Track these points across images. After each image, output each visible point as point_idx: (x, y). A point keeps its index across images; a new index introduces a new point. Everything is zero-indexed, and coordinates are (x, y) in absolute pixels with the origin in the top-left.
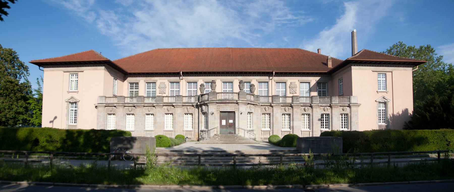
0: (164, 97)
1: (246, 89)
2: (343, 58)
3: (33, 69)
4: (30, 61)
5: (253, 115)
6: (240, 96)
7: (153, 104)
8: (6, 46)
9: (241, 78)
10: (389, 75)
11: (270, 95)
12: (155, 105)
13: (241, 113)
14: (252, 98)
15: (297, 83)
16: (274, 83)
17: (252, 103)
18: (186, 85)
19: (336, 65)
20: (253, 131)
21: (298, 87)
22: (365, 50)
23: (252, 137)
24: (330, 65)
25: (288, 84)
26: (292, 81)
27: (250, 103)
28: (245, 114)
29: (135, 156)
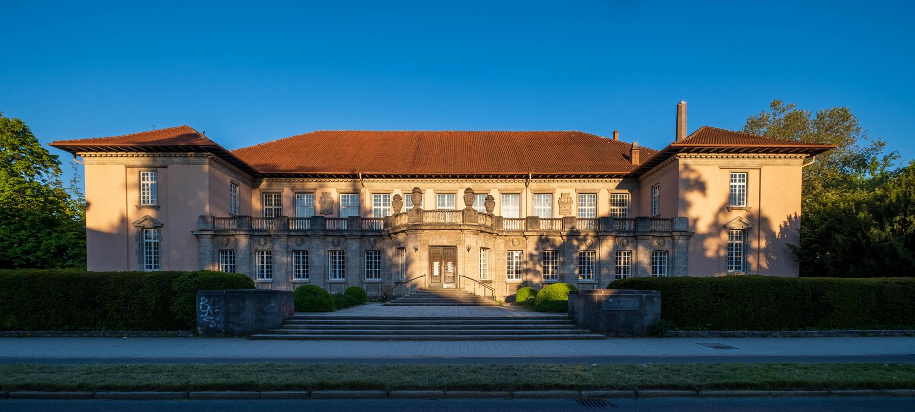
0: (326, 219)
1: (479, 205)
2: (658, 147)
4: (51, 143)
5: (490, 254)
6: (467, 218)
8: (11, 116)
9: (468, 184)
10: (753, 175)
11: (524, 216)
12: (309, 233)
13: (468, 250)
14: (489, 222)
15: (574, 196)
16: (530, 194)
17: (488, 230)
18: (371, 199)
20: (490, 282)
21: (575, 202)
22: (707, 128)
23: (489, 293)
24: (636, 161)
25: (557, 196)
26: (564, 191)
28: (475, 253)
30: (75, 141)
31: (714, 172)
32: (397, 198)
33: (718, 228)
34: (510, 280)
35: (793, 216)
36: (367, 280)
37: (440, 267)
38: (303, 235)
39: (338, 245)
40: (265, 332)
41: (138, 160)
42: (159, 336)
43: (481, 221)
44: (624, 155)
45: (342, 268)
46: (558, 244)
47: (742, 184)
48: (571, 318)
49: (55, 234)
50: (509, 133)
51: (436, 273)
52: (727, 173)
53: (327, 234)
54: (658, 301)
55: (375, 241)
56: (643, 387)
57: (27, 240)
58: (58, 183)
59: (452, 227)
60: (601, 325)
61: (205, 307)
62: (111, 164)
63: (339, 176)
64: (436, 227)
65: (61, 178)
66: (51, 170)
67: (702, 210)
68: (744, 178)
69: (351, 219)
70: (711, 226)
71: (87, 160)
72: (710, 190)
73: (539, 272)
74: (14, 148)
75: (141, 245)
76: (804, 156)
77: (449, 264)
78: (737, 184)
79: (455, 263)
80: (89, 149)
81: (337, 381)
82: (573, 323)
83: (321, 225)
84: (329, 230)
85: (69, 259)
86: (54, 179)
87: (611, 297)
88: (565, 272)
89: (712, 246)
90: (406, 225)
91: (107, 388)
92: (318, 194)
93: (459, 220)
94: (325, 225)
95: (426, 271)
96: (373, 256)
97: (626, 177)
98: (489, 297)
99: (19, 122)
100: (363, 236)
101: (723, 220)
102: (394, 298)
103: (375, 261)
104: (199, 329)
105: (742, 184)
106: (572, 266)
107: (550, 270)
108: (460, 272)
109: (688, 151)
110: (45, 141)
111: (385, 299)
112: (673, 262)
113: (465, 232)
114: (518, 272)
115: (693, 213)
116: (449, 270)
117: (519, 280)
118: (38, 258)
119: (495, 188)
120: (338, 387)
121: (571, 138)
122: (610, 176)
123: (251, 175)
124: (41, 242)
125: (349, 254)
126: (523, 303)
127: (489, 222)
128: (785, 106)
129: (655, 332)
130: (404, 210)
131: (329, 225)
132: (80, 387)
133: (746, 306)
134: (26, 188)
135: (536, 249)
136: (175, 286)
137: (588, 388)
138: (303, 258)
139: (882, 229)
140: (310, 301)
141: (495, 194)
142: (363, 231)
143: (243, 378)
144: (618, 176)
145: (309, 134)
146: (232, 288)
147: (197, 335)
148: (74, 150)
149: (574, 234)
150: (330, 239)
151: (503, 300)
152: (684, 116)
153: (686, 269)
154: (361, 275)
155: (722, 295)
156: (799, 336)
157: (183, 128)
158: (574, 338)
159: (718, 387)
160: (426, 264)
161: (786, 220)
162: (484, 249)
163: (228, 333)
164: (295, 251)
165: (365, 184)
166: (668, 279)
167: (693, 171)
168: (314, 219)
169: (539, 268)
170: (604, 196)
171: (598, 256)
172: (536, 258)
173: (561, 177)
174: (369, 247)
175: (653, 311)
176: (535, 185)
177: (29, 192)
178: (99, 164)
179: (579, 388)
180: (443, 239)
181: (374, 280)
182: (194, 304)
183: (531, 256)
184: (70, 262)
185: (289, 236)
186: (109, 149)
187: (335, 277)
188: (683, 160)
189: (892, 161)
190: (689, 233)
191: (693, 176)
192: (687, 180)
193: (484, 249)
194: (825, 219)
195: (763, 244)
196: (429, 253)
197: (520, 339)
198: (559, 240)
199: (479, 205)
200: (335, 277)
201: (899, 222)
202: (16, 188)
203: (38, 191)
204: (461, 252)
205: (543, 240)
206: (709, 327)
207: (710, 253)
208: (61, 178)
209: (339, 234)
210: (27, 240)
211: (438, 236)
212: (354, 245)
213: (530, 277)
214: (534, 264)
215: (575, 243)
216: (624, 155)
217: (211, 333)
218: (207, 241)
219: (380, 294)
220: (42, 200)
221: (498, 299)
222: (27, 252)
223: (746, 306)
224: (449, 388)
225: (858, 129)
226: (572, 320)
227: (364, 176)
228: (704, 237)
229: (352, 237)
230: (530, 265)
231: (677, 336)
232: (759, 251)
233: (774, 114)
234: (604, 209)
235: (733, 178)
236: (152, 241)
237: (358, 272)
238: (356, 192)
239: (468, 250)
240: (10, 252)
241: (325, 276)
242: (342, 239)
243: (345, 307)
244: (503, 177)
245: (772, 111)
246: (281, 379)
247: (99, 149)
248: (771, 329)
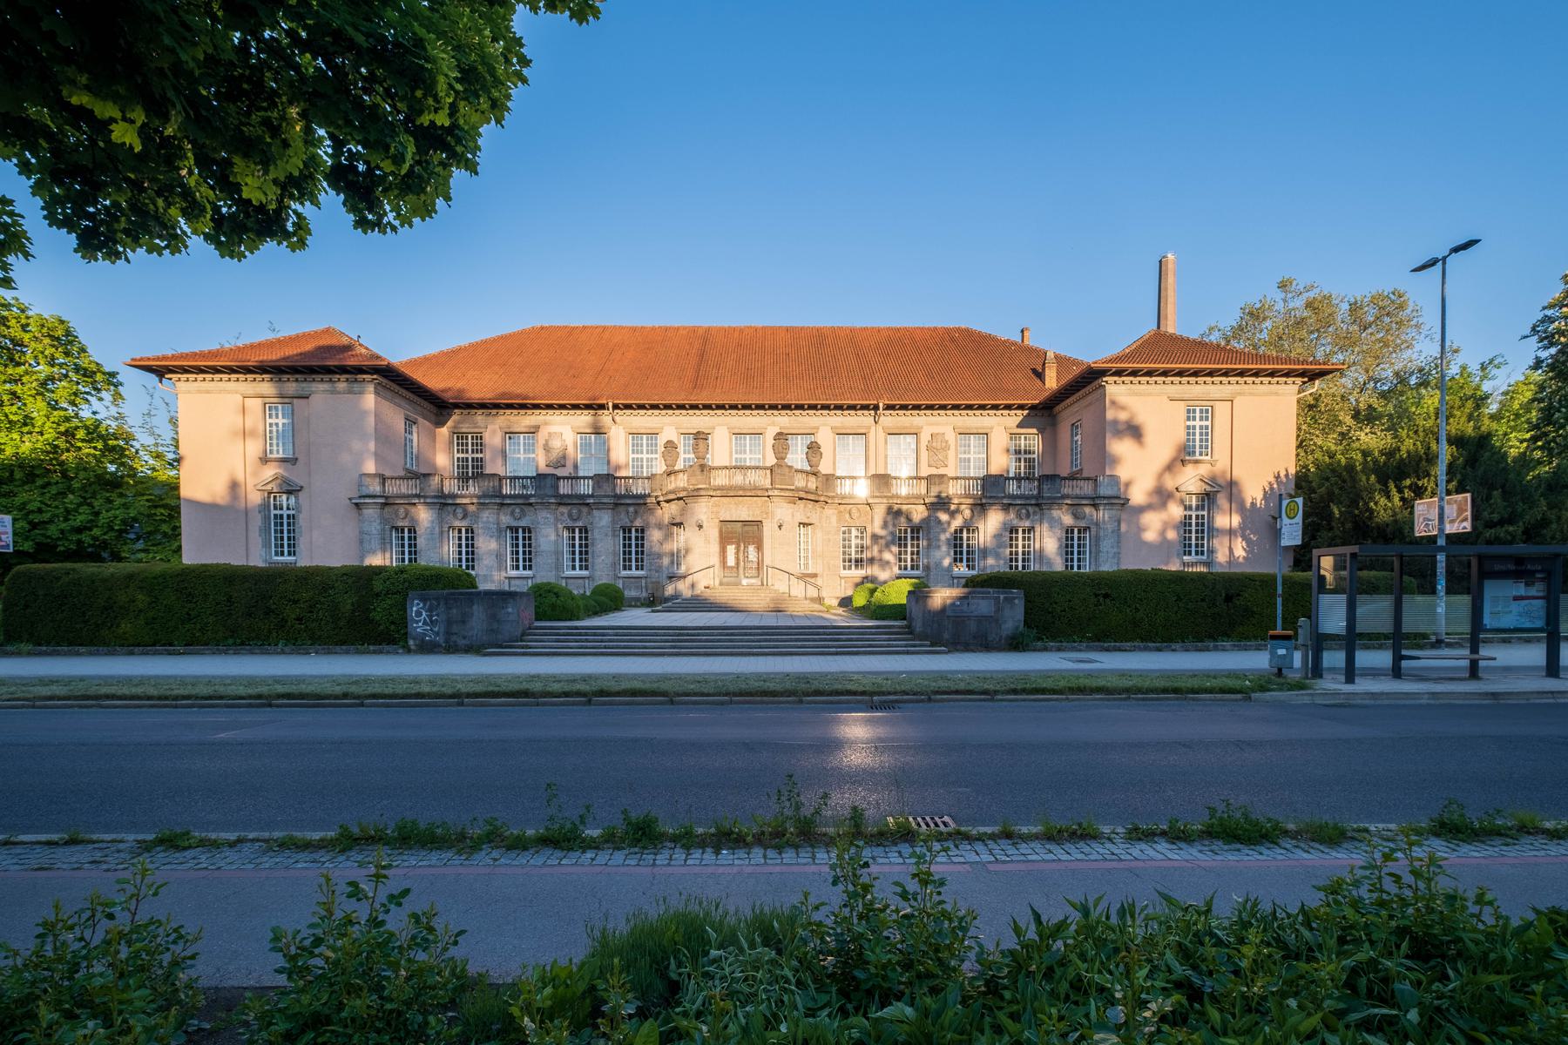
0: (559, 478)
1: (797, 457)
3: (134, 382)
4: (128, 361)
6: (777, 478)
7: (527, 497)
9: (783, 421)
10: (1222, 410)
12: (532, 500)
14: (812, 484)
15: (951, 436)
16: (881, 435)
18: (627, 442)
19: (1068, 378)
20: (815, 576)
21: (953, 447)
24: (1052, 382)
25: (925, 437)
26: (936, 430)
27: (802, 495)
29: (639, 488)
30: (165, 358)
31: (1153, 405)
32: (670, 445)
33: (1162, 496)
34: (847, 573)
35: (1283, 474)
37: (737, 553)
38: (524, 503)
40: (501, 647)
41: (266, 387)
42: (358, 652)
43: (800, 482)
44: (1034, 371)
45: (585, 552)
47: (1204, 423)
48: (909, 627)
49: (118, 502)
50: (852, 330)
51: (731, 561)
52: (1182, 406)
53: (563, 501)
54: (1020, 604)
56: (937, 693)
57: (76, 510)
58: (120, 417)
59: (752, 492)
60: (946, 636)
61: (419, 614)
62: (220, 392)
63: (576, 407)
64: (729, 492)
65: (126, 409)
66: (104, 394)
67: (1136, 468)
68: (1208, 414)
69: (599, 479)
70: (1150, 494)
71: (182, 386)
72: (1150, 436)
73: (888, 562)
74: (52, 362)
75: (266, 518)
76: (1299, 380)
77: (751, 549)
78: (1197, 423)
79: (759, 548)
80: (184, 370)
81: (617, 688)
82: (911, 633)
83: (547, 488)
84: (564, 496)
85: (138, 539)
86: (113, 411)
87: (960, 598)
89: (1154, 526)
90: (684, 489)
91: (374, 696)
92: (542, 436)
93: (767, 483)
94: (558, 488)
95: (715, 560)
96: (633, 534)
97: (1033, 408)
98: (812, 600)
99: (62, 322)
100: (616, 505)
101: (1170, 483)
102: (667, 600)
103: (634, 544)
104: (411, 642)
105: (1204, 423)
107: (1020, 543)
108: (767, 561)
109: (1119, 373)
110: (104, 351)
111: (654, 601)
112: (1097, 545)
114: (859, 562)
115: (1123, 473)
117: (861, 573)
118: (95, 538)
119: (824, 426)
120: (618, 694)
121: (953, 340)
122: (1008, 407)
123: (438, 406)
124: (97, 514)
125: (596, 532)
126: (858, 609)
127: (812, 484)
128: (1301, 287)
129: (1016, 644)
130: (680, 465)
131: (564, 488)
132: (345, 696)
133: (1137, 610)
134: (77, 428)
135: (885, 525)
136: (378, 586)
137: (883, 693)
138: (523, 544)
139: (1389, 497)
140: (552, 605)
141: (825, 438)
142: (616, 496)
143: (516, 687)
144: (1021, 407)
145: (523, 332)
146: (451, 587)
147: (409, 651)
148: (160, 371)
149: (942, 503)
150: (564, 510)
151: (835, 603)
152: (1170, 280)
153: (1117, 555)
154: (614, 565)
155: (1106, 596)
156: (1207, 649)
157: (327, 331)
158: (908, 653)
159: (1015, 691)
160: (715, 547)
161: (1272, 480)
162: (805, 525)
163: (451, 648)
164: (511, 528)
165: (617, 418)
166: (1034, 573)
167: (1123, 408)
168: (540, 478)
170: (993, 442)
172: (883, 542)
173: (930, 407)
174: (626, 522)
175: (1014, 616)
176: (889, 420)
177: (81, 434)
178: (199, 392)
179: (872, 694)
180: (742, 511)
181: (521, 572)
182: (403, 608)
183: (875, 537)
184: (140, 545)
185: (502, 504)
186: (216, 370)
188: (1116, 390)
189: (1495, 371)
190: (1119, 502)
191: (1123, 416)
192: (1115, 422)
193: (805, 525)
194: (1327, 479)
195: (1236, 520)
196: (721, 532)
197: (837, 654)
199: (797, 457)
200: (574, 568)
201: (1410, 487)
202: (62, 429)
203: (94, 431)
204: (769, 530)
205: (894, 513)
206: (1089, 639)
207: (1150, 536)
208: (126, 409)
209: (580, 502)
210: (76, 510)
212: (603, 519)
216: (1034, 371)
217: (427, 648)
218: (370, 513)
219: (644, 595)
220: (100, 445)
221: (827, 602)
222: (79, 530)
223: (1137, 610)
224: (735, 694)
225: (1418, 326)
226: (909, 630)
227: (616, 407)
228: (1141, 509)
229: (600, 506)
230: (875, 551)
231: (1045, 649)
232: (1231, 532)
233: (1285, 301)
234: (1001, 463)
235: (1190, 414)
236: (285, 513)
237: (609, 560)
238: (598, 431)
240: (53, 530)
241: (558, 567)
242: (585, 510)
243: (596, 614)
244: (839, 407)
245: (1279, 295)
246: (556, 687)
247: (200, 370)
248: (1171, 640)
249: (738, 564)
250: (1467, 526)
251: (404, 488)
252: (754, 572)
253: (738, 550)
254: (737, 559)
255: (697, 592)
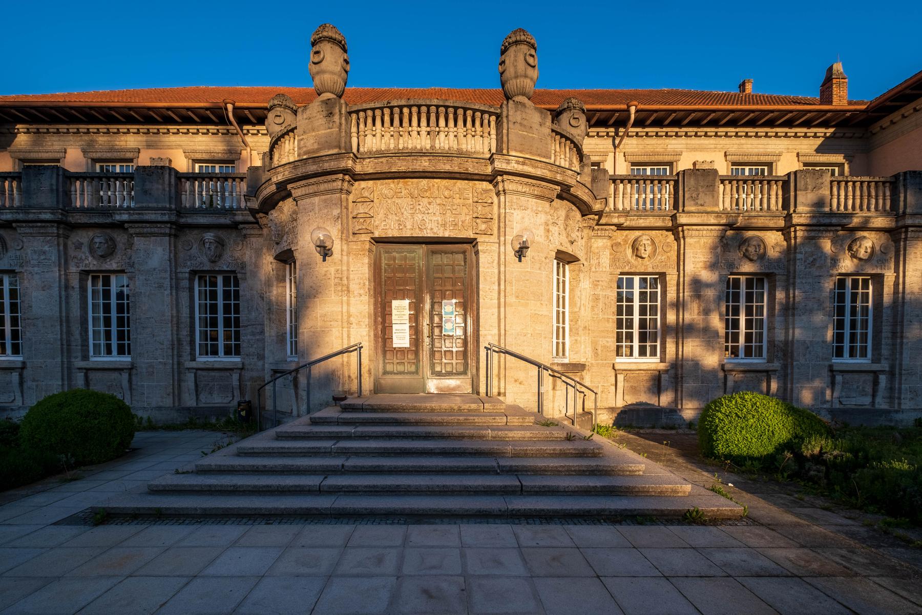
13: (521, 253)
20: (579, 367)
28: (540, 268)
36: (204, 360)
37: (415, 319)
39: (109, 253)
46: (773, 253)
51: (401, 338)
55: (221, 243)
73: (716, 334)
77: (450, 308)
79: (470, 305)
88: (798, 334)
95: (362, 333)
106: (819, 318)
108: (488, 336)
113: (510, 184)
116: (448, 327)
117: (652, 363)
135: (712, 266)
154: (177, 345)
160: (361, 304)
165: (249, 139)
169: (717, 323)
171: (888, 289)
172: (710, 293)
174: (203, 262)
181: (222, 359)
183: (697, 285)
187: (109, 352)
198: (774, 241)
205: (734, 237)
211: (405, 202)
212: (154, 253)
213: (692, 348)
214: (706, 312)
215: (827, 246)
230: (692, 315)
237: (166, 335)
239: (521, 253)
242: (120, 238)
249: (416, 340)
250: (395, 303)
251: (501, 188)
252: (456, 363)
253: (417, 308)
254: (416, 331)
255: (751, 452)
